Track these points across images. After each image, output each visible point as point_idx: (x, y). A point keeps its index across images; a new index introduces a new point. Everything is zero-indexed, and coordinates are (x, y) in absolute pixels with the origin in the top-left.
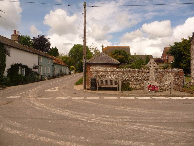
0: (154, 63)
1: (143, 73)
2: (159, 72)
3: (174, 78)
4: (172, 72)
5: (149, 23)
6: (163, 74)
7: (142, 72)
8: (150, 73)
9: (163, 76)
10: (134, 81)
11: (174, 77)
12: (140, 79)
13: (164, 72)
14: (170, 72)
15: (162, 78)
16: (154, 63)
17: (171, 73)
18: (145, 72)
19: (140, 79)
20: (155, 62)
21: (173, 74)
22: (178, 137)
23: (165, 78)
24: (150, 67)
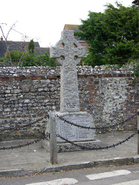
0: (76, 46)
1: (35, 81)
2: (86, 76)
3: (126, 94)
4: (120, 75)
5: (134, 180)
6: (97, 83)
7: (33, 77)
8: (62, 81)
9: (98, 89)
10: (8, 110)
11: (127, 89)
12: (27, 101)
13: (100, 76)
14: (115, 75)
15: (95, 94)
16: (76, 46)
17: (118, 79)
18: (43, 78)
19: (27, 101)
20: (77, 42)
21: (123, 83)
22: (115, 155)
23: (103, 94)
24: (63, 57)
